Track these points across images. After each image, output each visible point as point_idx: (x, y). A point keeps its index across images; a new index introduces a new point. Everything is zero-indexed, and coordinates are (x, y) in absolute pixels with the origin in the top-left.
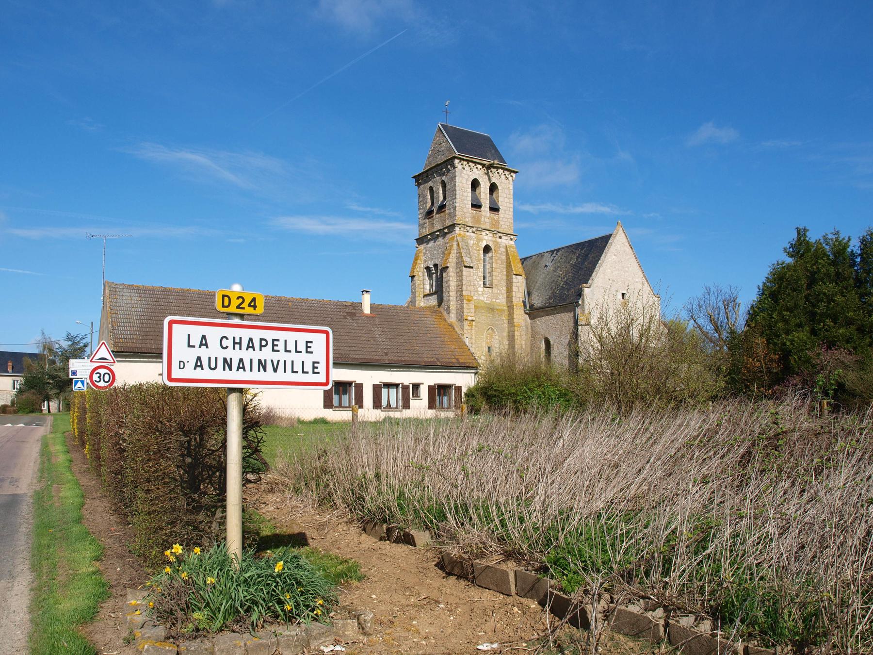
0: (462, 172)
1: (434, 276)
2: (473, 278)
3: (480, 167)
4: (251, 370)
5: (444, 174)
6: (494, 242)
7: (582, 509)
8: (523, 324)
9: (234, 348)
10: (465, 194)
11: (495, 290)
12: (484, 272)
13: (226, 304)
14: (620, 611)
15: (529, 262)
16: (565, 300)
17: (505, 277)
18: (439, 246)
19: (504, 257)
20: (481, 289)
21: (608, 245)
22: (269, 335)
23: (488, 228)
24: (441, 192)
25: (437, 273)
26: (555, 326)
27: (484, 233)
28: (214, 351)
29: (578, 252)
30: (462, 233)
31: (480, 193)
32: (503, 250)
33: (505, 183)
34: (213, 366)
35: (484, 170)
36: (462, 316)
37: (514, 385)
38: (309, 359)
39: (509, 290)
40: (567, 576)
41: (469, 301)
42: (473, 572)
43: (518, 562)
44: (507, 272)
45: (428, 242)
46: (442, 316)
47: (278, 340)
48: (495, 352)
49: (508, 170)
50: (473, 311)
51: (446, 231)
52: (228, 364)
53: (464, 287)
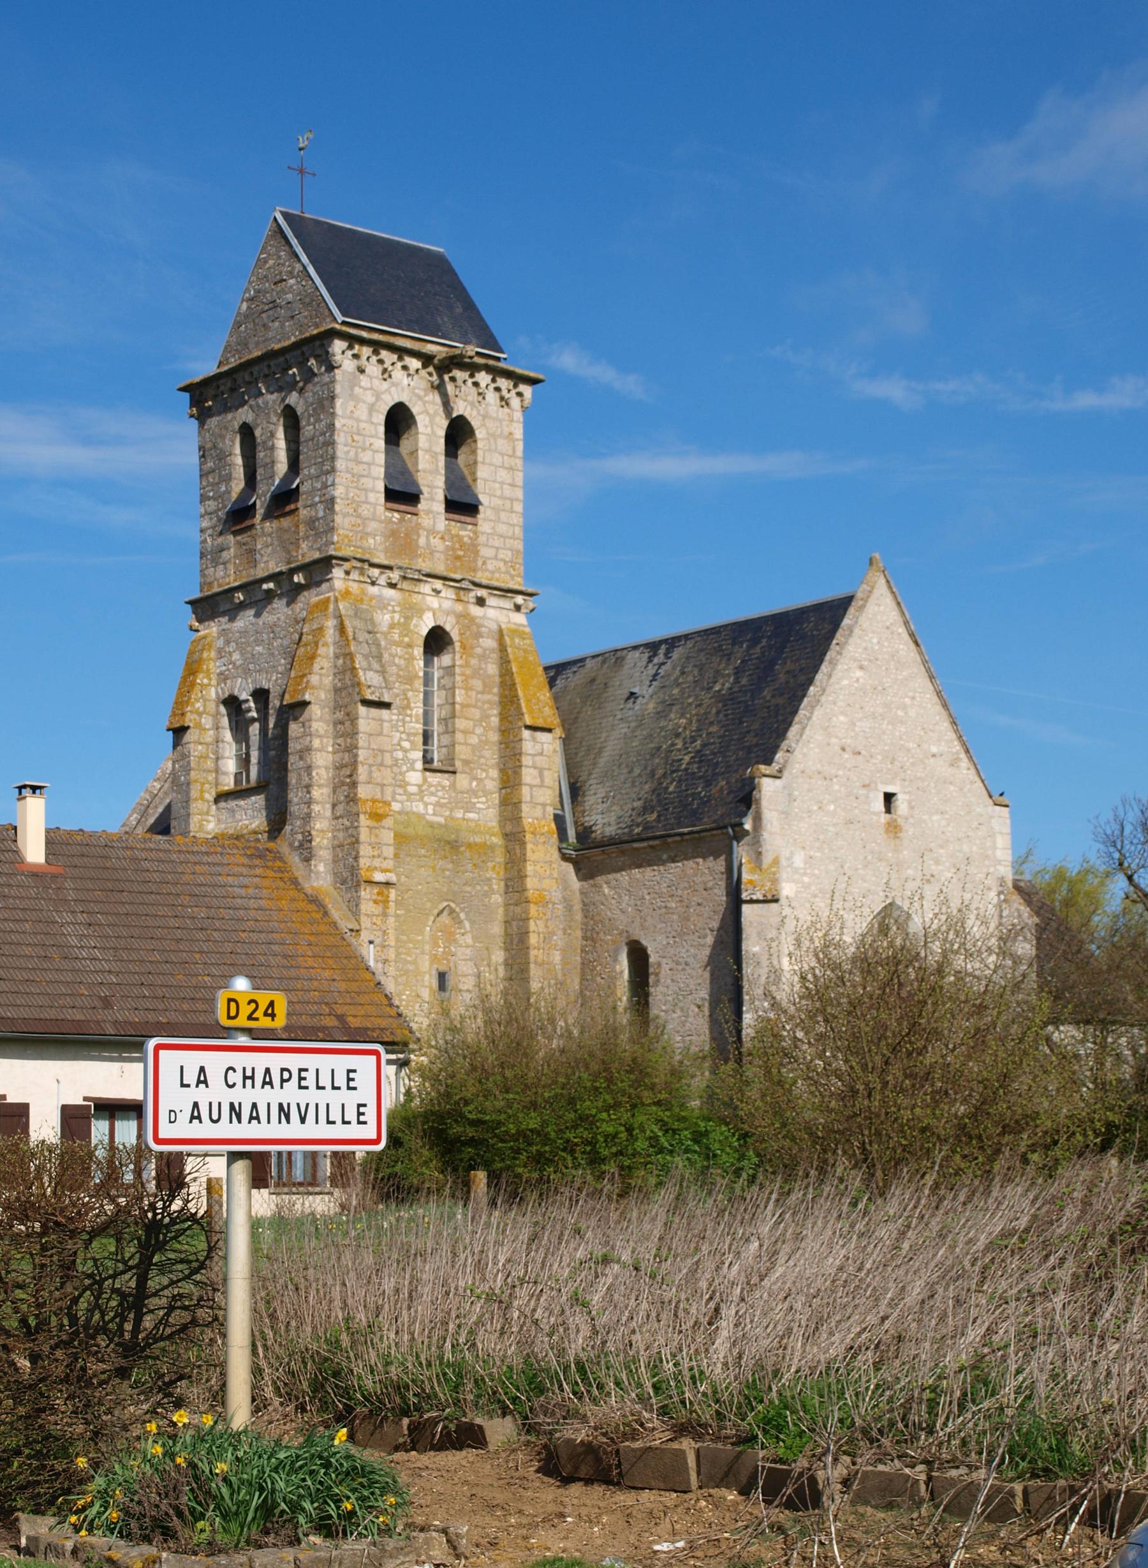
0: (353, 383)
1: (254, 729)
2: (389, 738)
3: (414, 364)
4: (269, 1122)
5: (292, 386)
6: (460, 616)
7: (801, 1356)
8: (556, 895)
9: (244, 1086)
10: (366, 457)
11: (462, 781)
12: (427, 718)
13: (233, 1013)
14: (865, 1473)
15: (572, 680)
16: (695, 817)
17: (494, 737)
18: (272, 628)
19: (492, 669)
20: (415, 777)
21: (839, 636)
22: (294, 1061)
23: (440, 569)
24: (281, 443)
25: (268, 725)
26: (665, 902)
27: (426, 588)
28: (216, 1093)
29: (740, 652)
30: (354, 587)
31: (414, 453)
32: (490, 643)
33: (499, 419)
34: (215, 1117)
35: (426, 377)
36: (354, 870)
37: (534, 1105)
38: (351, 1100)
39: (510, 780)
40: (784, 1441)
41: (378, 817)
42: (619, 1466)
43: (698, 1437)
44: (503, 717)
45: (233, 612)
46: (283, 872)
47: (306, 1070)
48: (465, 982)
49: (508, 375)
50: (389, 851)
51: (298, 578)
52: (235, 1111)
53: (362, 772)
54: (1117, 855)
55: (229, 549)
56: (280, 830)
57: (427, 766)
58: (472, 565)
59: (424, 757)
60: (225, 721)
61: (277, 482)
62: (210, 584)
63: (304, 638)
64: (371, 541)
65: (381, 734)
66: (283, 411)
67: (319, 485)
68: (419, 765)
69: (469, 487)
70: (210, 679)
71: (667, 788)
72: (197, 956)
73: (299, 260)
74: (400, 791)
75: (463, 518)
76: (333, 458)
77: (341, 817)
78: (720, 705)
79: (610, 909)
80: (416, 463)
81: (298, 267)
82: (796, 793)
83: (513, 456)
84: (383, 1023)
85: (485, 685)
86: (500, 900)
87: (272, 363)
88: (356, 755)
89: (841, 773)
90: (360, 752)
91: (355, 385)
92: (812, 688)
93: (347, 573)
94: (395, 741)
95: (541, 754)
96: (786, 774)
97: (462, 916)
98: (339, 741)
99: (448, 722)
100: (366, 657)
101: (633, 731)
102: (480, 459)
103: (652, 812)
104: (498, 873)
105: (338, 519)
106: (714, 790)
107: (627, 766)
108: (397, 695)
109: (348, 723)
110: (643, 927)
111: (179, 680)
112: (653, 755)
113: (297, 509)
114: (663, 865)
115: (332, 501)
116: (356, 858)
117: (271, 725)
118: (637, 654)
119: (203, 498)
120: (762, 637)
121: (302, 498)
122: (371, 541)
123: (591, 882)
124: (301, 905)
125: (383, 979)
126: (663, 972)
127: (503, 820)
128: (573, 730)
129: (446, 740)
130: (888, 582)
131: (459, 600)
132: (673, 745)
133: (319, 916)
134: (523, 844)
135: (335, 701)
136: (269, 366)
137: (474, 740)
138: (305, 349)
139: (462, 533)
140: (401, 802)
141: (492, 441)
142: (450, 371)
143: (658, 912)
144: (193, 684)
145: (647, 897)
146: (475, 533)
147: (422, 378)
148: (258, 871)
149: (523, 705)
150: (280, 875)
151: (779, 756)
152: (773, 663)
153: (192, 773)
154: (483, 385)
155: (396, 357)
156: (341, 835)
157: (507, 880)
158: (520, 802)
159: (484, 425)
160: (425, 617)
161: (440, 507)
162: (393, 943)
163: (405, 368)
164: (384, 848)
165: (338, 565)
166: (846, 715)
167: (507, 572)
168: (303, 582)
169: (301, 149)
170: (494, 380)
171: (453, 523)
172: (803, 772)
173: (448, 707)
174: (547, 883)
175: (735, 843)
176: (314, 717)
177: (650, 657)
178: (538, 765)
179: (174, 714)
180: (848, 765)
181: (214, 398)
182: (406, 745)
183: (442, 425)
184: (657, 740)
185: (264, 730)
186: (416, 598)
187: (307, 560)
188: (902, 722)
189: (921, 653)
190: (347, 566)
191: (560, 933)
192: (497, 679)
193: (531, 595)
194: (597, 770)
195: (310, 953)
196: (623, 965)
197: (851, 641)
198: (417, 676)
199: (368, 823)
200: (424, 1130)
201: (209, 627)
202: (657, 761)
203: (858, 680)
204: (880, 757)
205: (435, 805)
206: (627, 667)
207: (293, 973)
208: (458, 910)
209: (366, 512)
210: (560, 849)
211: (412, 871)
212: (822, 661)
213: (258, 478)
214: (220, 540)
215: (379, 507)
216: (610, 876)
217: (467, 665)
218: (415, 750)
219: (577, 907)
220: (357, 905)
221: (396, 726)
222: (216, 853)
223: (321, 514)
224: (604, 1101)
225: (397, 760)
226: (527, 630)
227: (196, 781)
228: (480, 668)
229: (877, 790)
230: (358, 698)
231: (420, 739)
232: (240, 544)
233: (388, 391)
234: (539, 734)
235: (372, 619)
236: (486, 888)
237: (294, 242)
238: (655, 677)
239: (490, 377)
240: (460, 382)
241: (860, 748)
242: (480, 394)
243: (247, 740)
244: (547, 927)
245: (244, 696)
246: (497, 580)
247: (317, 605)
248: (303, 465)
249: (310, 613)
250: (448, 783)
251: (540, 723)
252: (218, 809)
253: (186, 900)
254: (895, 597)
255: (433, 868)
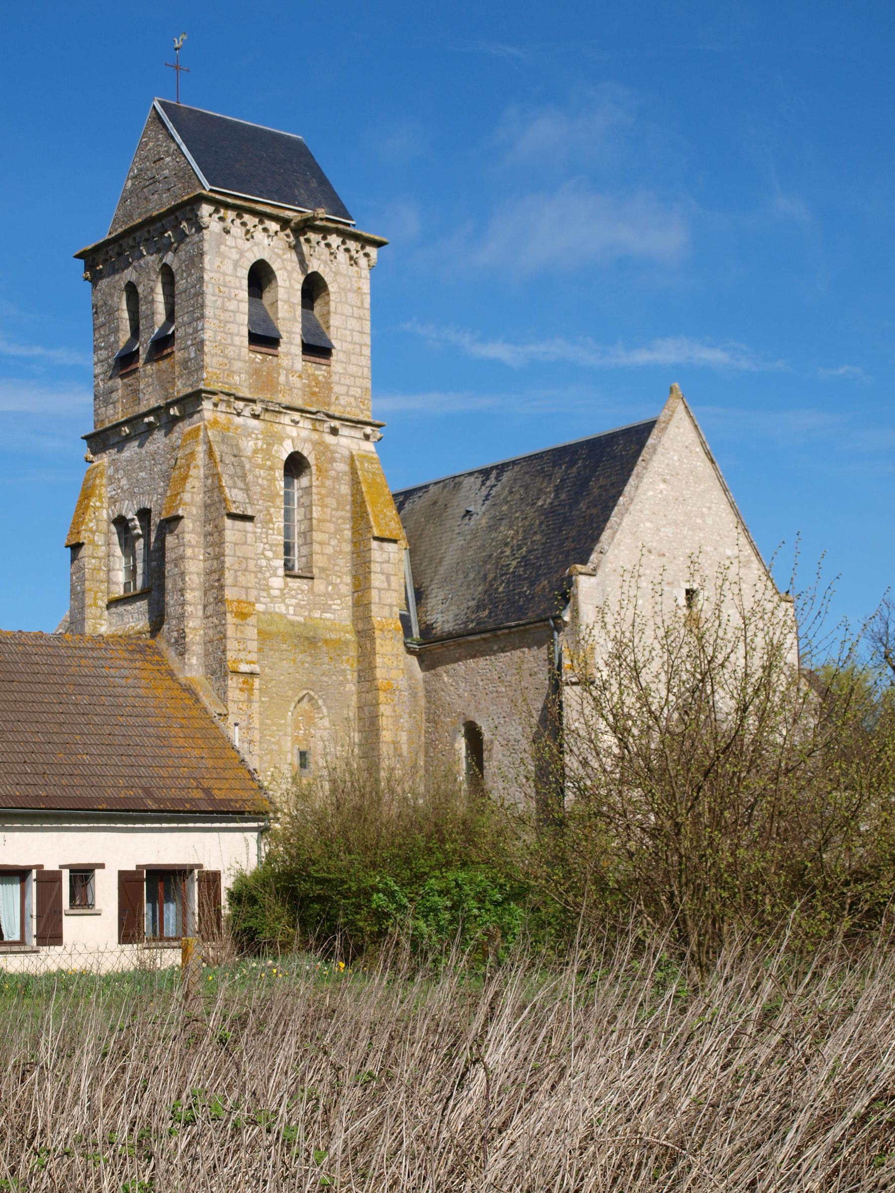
0: (220, 243)
1: (140, 544)
2: (255, 549)
3: (274, 226)
5: (168, 247)
6: (315, 444)
8: (403, 684)
10: (232, 305)
11: (319, 585)
12: (288, 531)
15: (418, 504)
17: (347, 548)
18: (153, 456)
19: (345, 489)
21: (645, 454)
23: (298, 403)
24: (159, 298)
25: (148, 536)
26: (494, 688)
27: (286, 419)
29: (559, 473)
30: (222, 418)
31: (274, 303)
32: (342, 467)
33: (350, 278)
36: (222, 662)
41: (243, 616)
44: (355, 531)
45: (120, 445)
49: (356, 237)
50: (254, 646)
54: (883, 649)
55: (117, 390)
56: (159, 630)
57: (288, 572)
58: (327, 400)
59: (285, 565)
60: (115, 539)
61: (156, 330)
62: (102, 421)
63: (178, 463)
64: (237, 378)
65: (245, 543)
66: (161, 269)
67: (191, 331)
68: (281, 572)
69: (323, 333)
70: (102, 502)
71: (497, 589)
72: (78, 737)
73: (174, 140)
74: (264, 594)
75: (318, 360)
76: (202, 306)
77: (211, 616)
78: (543, 517)
79: (449, 695)
80: (276, 312)
81: (173, 146)
82: (609, 589)
83: (361, 307)
84: (246, 795)
85: (338, 503)
86: (353, 688)
87: (151, 229)
88: (224, 562)
89: (648, 572)
90: (227, 559)
91: (221, 244)
92: (621, 498)
93: (216, 405)
94: (260, 551)
95: (388, 562)
96: (599, 572)
97: (320, 702)
98: (209, 550)
99: (307, 535)
100: (231, 477)
101: (469, 543)
102: (332, 309)
103: (484, 610)
104: (352, 665)
105: (207, 359)
106: (538, 589)
107: (463, 572)
108: (260, 511)
109: (216, 535)
110: (477, 710)
111: (76, 504)
112: (485, 562)
113: (173, 352)
114: (494, 655)
115: (202, 342)
116: (224, 651)
117: (153, 540)
118: (472, 479)
119: (97, 349)
120: (579, 459)
121: (177, 342)
122: (237, 378)
123: (433, 672)
124: (175, 693)
125: (247, 758)
126: (495, 748)
127: (356, 619)
128: (418, 544)
129: (305, 550)
130: (686, 407)
131: (315, 430)
132: (502, 552)
133: (190, 703)
134: (373, 639)
135: (206, 515)
136: (149, 232)
137: (329, 550)
138: (177, 214)
139: (317, 373)
140: (266, 604)
141: (343, 294)
142: (305, 234)
143: (491, 696)
144: (87, 507)
145: (481, 683)
146: (329, 372)
147: (280, 239)
148: (138, 664)
149: (372, 519)
150: (158, 667)
151: (593, 557)
152: (587, 480)
153: (87, 583)
154: (334, 246)
155: (257, 220)
156: (211, 632)
157: (359, 671)
158: (370, 603)
159: (336, 281)
160: (285, 444)
161: (298, 350)
162: (257, 726)
163: (265, 230)
164: (249, 643)
165: (207, 398)
166: (652, 522)
167: (357, 407)
168: (178, 414)
169: (176, 49)
170: (344, 243)
171: (310, 364)
172: (615, 571)
173: (306, 522)
174: (394, 673)
175: (556, 633)
176: (186, 529)
177: (483, 481)
178: (386, 571)
179: (71, 533)
180: (654, 566)
181: (105, 262)
182: (269, 554)
183: (299, 279)
184: (489, 549)
185: (147, 545)
186: (277, 428)
187: (181, 395)
188: (700, 529)
189: (716, 469)
190: (215, 399)
191: (406, 716)
192: (349, 498)
193: (379, 426)
194: (438, 577)
195: (181, 735)
196: (461, 744)
197: (654, 458)
198: (278, 495)
199: (234, 620)
200: (277, 889)
201: (101, 458)
202: (489, 566)
203: (661, 491)
204: (682, 559)
205: (295, 607)
206: (463, 490)
207: (165, 751)
208: (316, 697)
209: (232, 353)
210: (405, 644)
211: (274, 663)
212: (629, 476)
213: (141, 328)
214: (110, 383)
215: (243, 349)
216: (449, 667)
217: (323, 485)
218: (277, 558)
219: (421, 693)
220: (225, 693)
221: (261, 538)
222: (101, 649)
223: (193, 355)
224: (437, 860)
225: (261, 567)
226: (376, 456)
227: (90, 590)
228: (334, 488)
229: (680, 587)
230: (224, 512)
231: (281, 549)
232: (126, 386)
233: (250, 249)
234: (386, 545)
235: (237, 445)
236: (341, 678)
237: (170, 125)
238: (487, 498)
239: (340, 240)
240: (314, 243)
241: (664, 551)
242: (331, 254)
243: (134, 554)
244: (394, 711)
245: (130, 516)
246: (349, 413)
247: (189, 434)
248: (177, 314)
249: (183, 440)
250: (306, 587)
251: (386, 535)
252: (109, 614)
253: (71, 689)
254: (693, 420)
255: (294, 660)
